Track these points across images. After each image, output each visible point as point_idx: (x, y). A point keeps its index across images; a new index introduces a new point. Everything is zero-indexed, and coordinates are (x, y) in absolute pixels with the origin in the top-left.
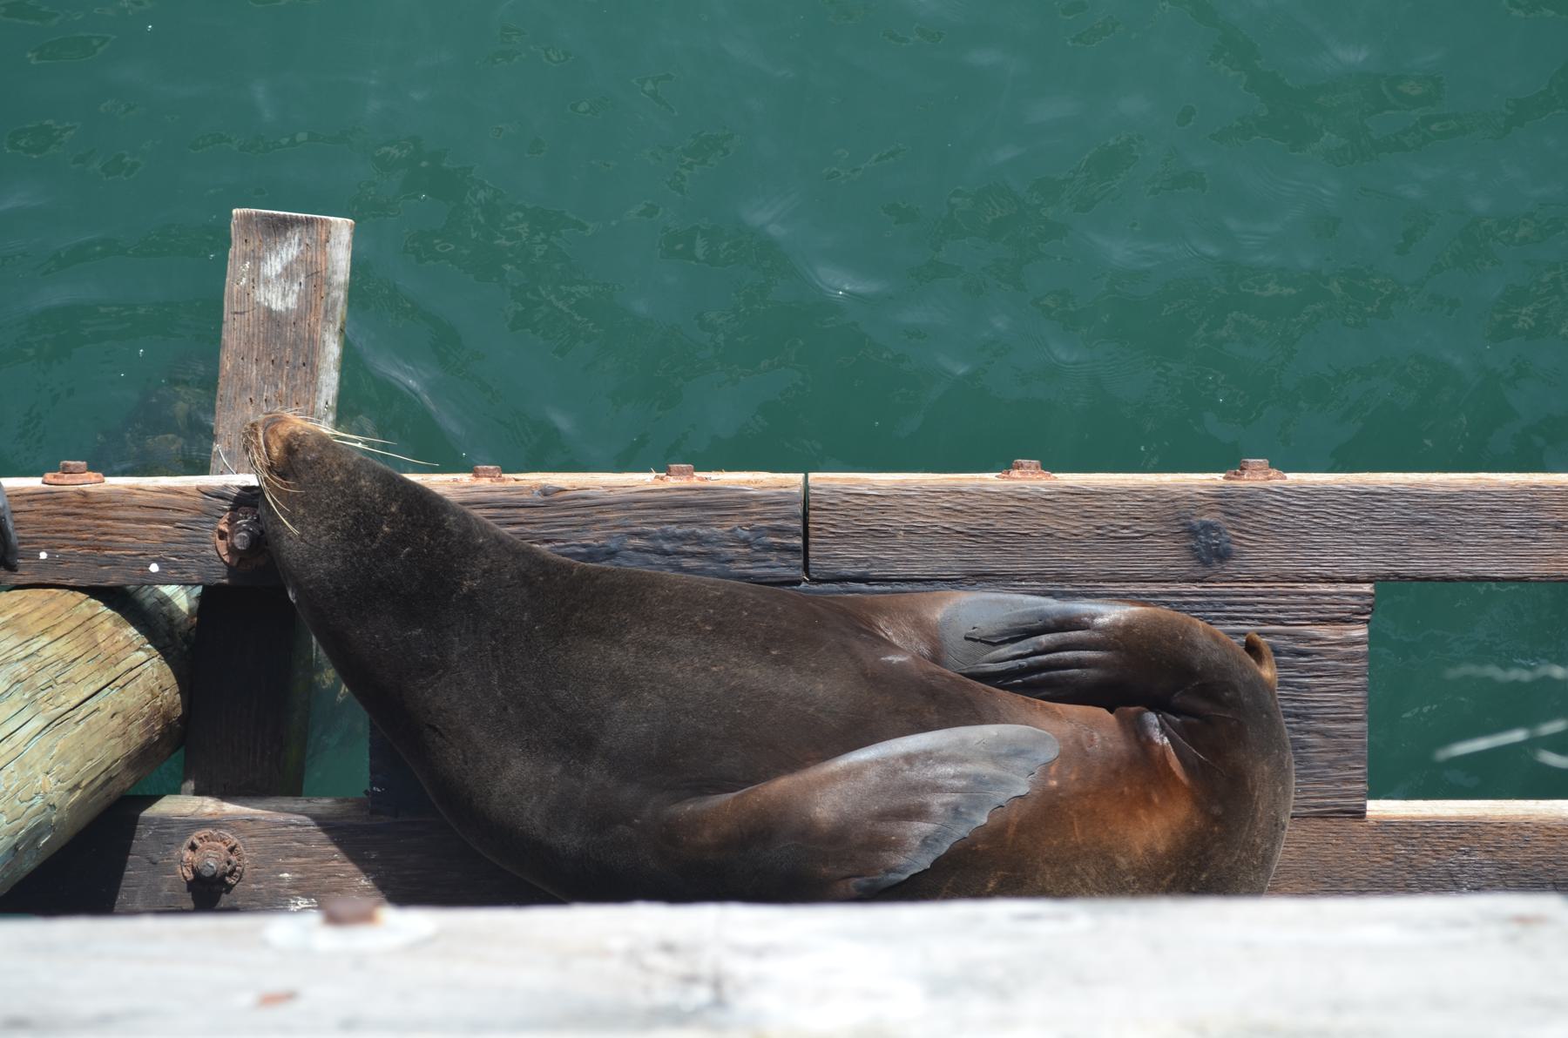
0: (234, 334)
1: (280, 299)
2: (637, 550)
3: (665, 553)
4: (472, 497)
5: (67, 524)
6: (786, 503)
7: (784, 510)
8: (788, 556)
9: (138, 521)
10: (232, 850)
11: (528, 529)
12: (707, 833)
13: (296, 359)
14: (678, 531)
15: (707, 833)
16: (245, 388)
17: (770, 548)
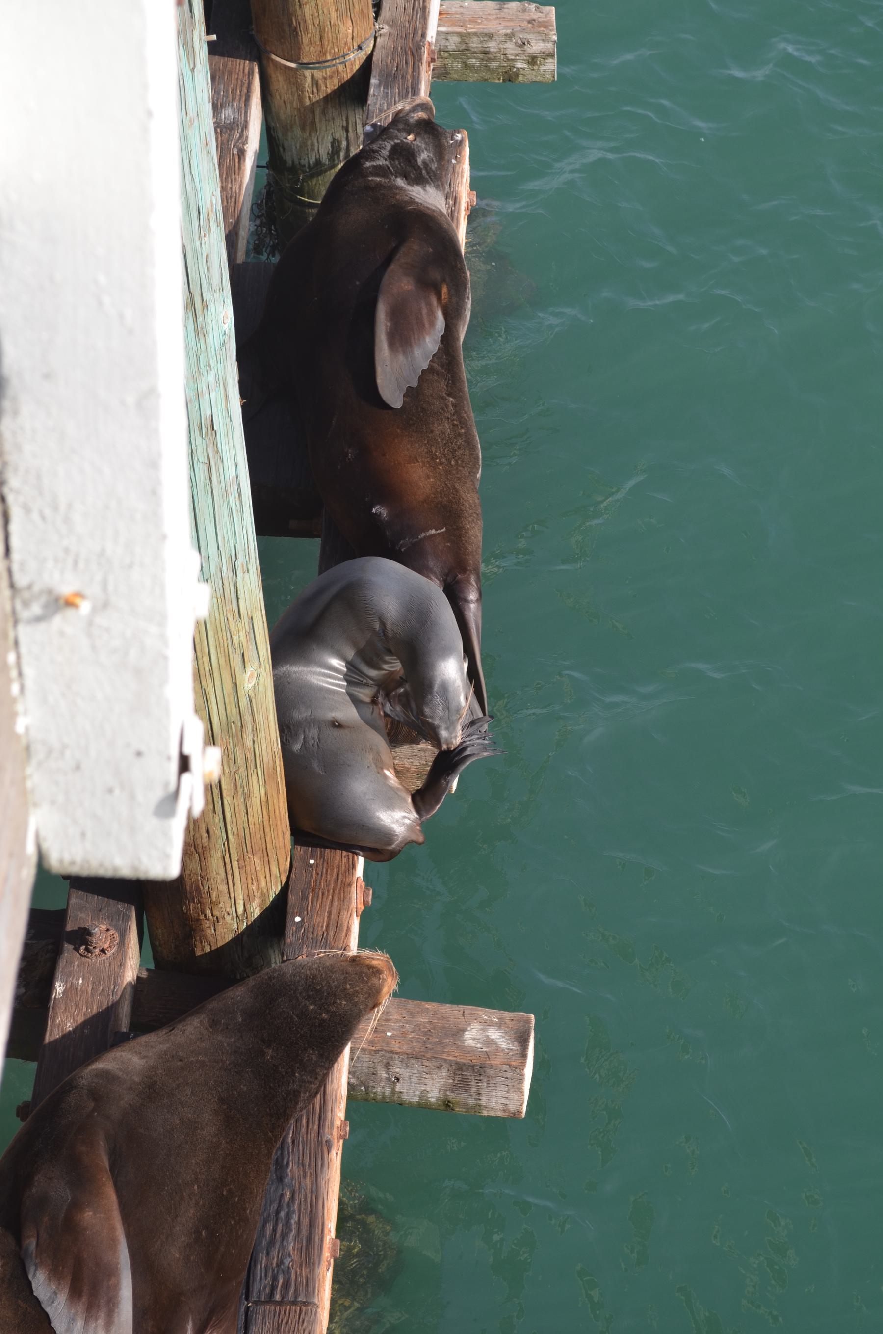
0: (451, 1011)
1: (472, 1036)
2: (282, 1195)
3: (277, 1212)
4: (328, 1097)
5: (332, 875)
6: (307, 1291)
7: (302, 1290)
8: (267, 1291)
9: (330, 913)
10: (103, 951)
11: (303, 1130)
12: (84, 1149)
13: (430, 1043)
14: (293, 1221)
15: (84, 1149)
16: (412, 1015)
17: (275, 1279)
